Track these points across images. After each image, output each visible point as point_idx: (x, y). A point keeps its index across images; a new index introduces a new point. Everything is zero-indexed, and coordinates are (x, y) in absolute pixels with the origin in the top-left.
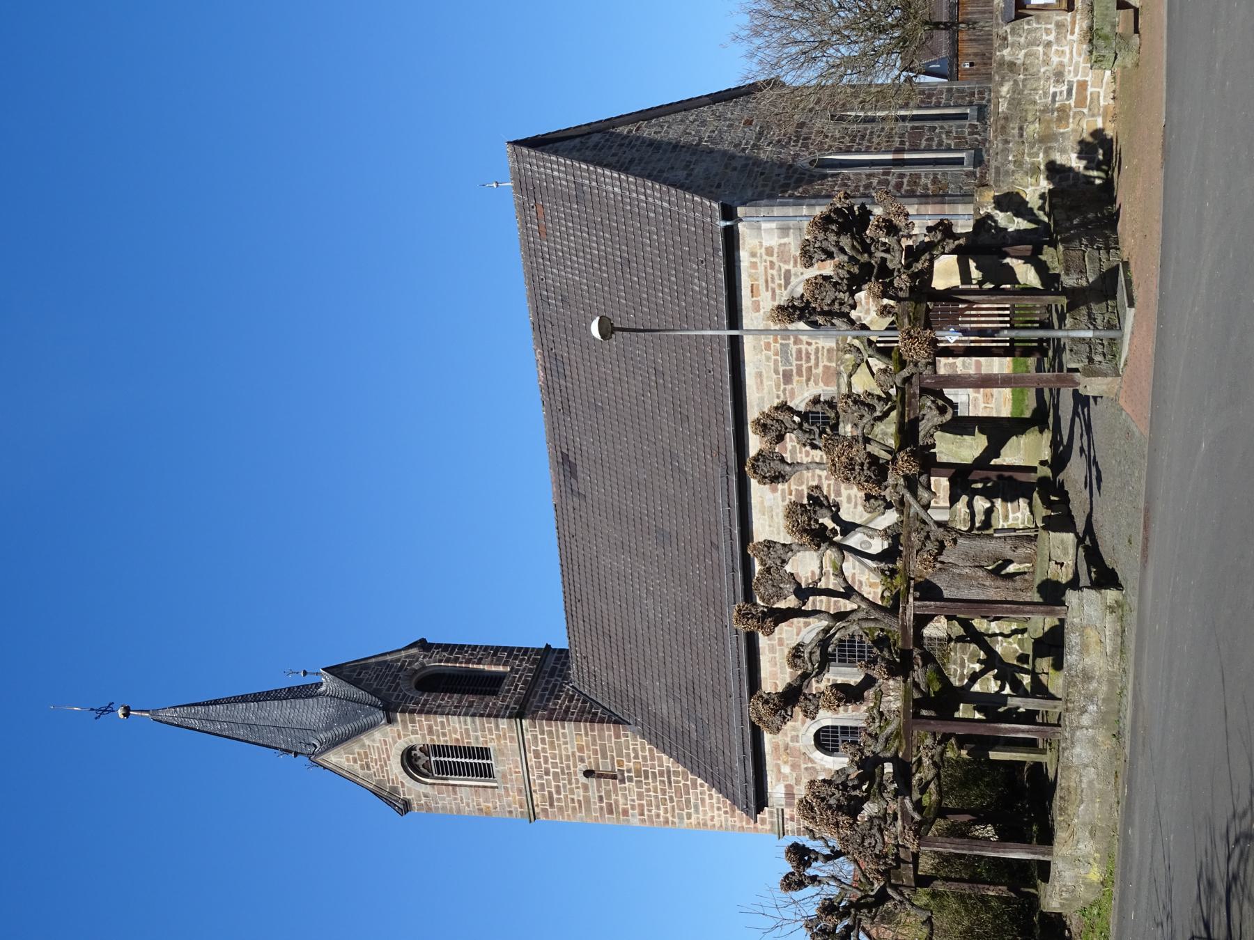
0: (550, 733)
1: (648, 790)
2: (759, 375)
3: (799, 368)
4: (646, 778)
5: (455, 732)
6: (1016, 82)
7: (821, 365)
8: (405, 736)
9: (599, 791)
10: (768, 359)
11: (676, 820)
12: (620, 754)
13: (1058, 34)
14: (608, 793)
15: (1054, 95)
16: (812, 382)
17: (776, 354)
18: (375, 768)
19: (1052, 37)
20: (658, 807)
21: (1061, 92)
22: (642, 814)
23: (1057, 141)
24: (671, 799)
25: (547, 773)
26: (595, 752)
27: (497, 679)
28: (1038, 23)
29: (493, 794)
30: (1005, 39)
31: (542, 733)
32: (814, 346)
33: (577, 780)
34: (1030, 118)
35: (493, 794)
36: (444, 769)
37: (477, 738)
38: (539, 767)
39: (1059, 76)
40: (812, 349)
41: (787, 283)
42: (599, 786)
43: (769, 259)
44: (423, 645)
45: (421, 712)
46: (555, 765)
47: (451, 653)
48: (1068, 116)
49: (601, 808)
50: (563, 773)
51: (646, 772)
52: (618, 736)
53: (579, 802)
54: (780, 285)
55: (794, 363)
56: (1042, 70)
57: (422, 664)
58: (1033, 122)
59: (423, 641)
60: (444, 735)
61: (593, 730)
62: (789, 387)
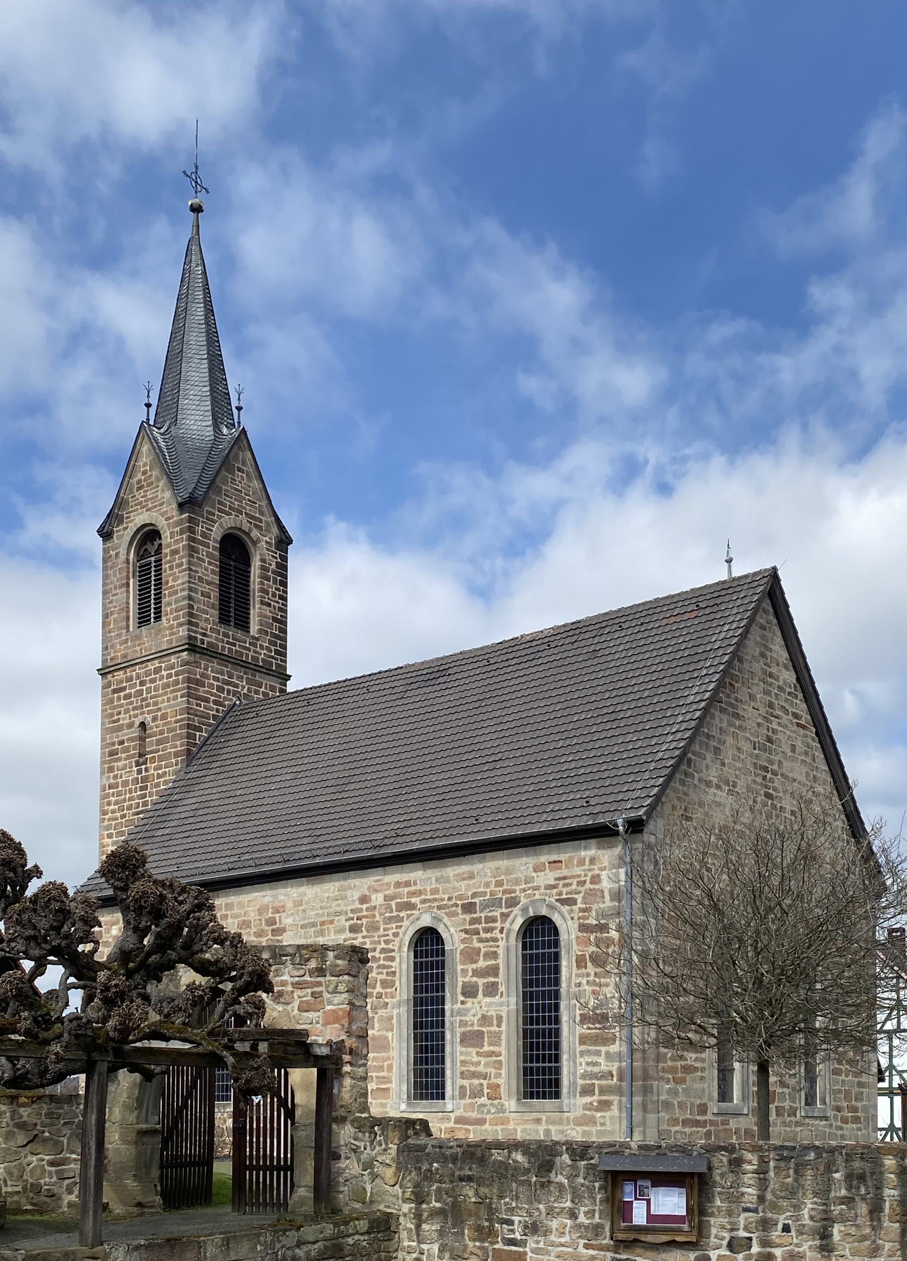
0: (176, 683)
1: (130, 792)
2: (471, 876)
3: (477, 921)
4: (142, 789)
5: (174, 580)
6: (527, 1171)
7: (481, 945)
8: (168, 525)
9: (128, 740)
10: (487, 885)
11: (106, 823)
12: (161, 759)
13: (587, 1228)
14: (126, 750)
15: (510, 1222)
16: (464, 935)
17: (492, 894)
18: (139, 495)
19: (582, 1219)
20: (116, 803)
21: (513, 1231)
22: (110, 788)
23: (454, 1226)
24: (123, 816)
25: (142, 683)
26: (162, 733)
27: (243, 624)
28: (601, 1202)
29: (121, 628)
30: (582, 1159)
31: (177, 674)
32: (499, 936)
33: (136, 716)
34: (483, 1190)
35: (121, 628)
36: (143, 573)
37: (169, 604)
38: (147, 674)
39: (533, 1228)
40: (496, 934)
41: (563, 902)
42: (131, 740)
43: (588, 879)
44: (284, 541)
45: (190, 539)
46: (149, 690)
47: (274, 572)
48: (482, 1241)
49: (113, 744)
50: (143, 700)
51: (146, 788)
52: (176, 755)
53: (118, 720)
54: (560, 894)
55: (483, 915)
56: (541, 1206)
57: (259, 540)
58: (477, 1194)
59: (290, 541)
60: (171, 568)
61: (181, 728)
62: (459, 910)
